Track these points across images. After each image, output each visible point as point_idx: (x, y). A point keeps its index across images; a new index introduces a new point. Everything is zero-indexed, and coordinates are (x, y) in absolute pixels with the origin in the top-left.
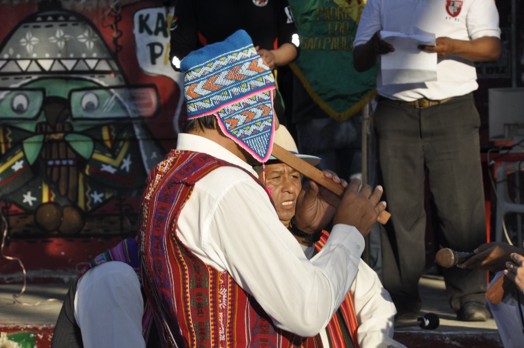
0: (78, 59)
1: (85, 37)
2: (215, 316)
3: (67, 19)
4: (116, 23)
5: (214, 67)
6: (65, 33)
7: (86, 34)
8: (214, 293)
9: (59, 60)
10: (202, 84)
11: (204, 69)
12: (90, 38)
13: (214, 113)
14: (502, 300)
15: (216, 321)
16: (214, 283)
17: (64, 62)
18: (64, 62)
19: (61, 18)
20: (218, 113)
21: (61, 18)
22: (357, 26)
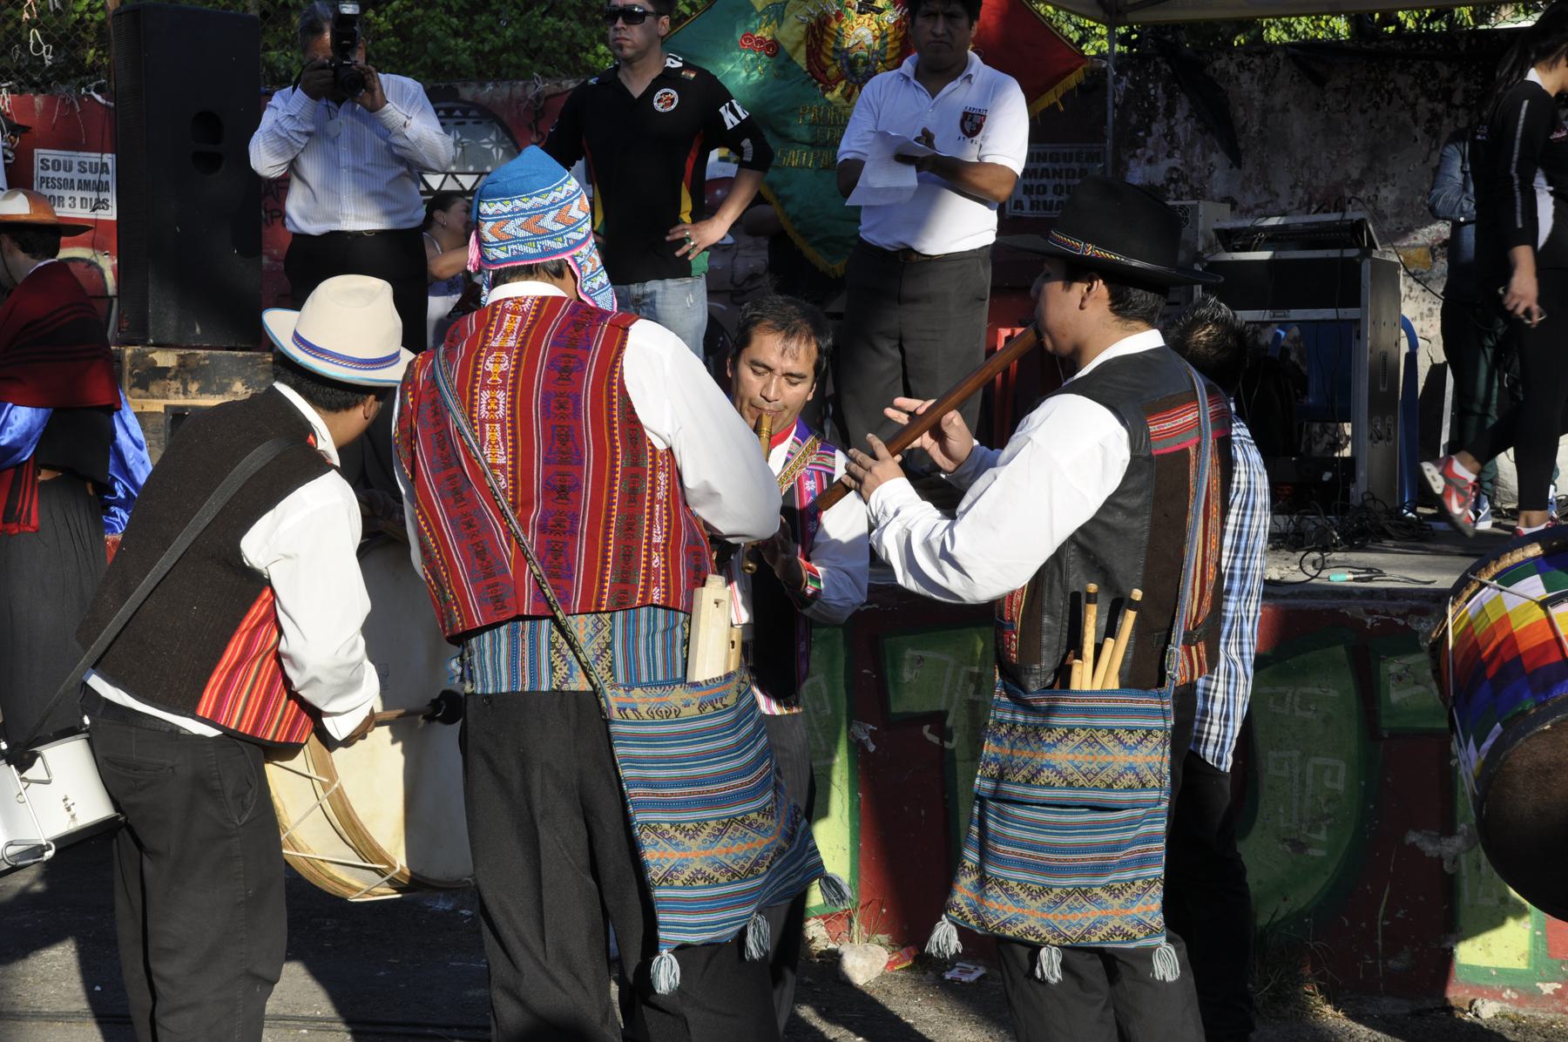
0: (481, 174)
1: (491, 142)
2: (652, 508)
3: (465, 115)
4: (536, 121)
5: (550, 199)
6: (463, 135)
7: (493, 137)
8: (653, 476)
9: (453, 175)
10: (552, 214)
11: (554, 194)
12: (498, 143)
13: (566, 257)
14: (94, 667)
15: (652, 513)
16: (654, 463)
17: (459, 177)
18: (459, 177)
19: (457, 113)
20: (573, 258)
21: (457, 113)
22: (847, 121)
